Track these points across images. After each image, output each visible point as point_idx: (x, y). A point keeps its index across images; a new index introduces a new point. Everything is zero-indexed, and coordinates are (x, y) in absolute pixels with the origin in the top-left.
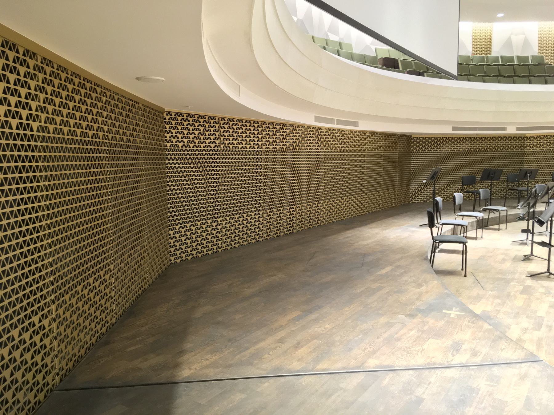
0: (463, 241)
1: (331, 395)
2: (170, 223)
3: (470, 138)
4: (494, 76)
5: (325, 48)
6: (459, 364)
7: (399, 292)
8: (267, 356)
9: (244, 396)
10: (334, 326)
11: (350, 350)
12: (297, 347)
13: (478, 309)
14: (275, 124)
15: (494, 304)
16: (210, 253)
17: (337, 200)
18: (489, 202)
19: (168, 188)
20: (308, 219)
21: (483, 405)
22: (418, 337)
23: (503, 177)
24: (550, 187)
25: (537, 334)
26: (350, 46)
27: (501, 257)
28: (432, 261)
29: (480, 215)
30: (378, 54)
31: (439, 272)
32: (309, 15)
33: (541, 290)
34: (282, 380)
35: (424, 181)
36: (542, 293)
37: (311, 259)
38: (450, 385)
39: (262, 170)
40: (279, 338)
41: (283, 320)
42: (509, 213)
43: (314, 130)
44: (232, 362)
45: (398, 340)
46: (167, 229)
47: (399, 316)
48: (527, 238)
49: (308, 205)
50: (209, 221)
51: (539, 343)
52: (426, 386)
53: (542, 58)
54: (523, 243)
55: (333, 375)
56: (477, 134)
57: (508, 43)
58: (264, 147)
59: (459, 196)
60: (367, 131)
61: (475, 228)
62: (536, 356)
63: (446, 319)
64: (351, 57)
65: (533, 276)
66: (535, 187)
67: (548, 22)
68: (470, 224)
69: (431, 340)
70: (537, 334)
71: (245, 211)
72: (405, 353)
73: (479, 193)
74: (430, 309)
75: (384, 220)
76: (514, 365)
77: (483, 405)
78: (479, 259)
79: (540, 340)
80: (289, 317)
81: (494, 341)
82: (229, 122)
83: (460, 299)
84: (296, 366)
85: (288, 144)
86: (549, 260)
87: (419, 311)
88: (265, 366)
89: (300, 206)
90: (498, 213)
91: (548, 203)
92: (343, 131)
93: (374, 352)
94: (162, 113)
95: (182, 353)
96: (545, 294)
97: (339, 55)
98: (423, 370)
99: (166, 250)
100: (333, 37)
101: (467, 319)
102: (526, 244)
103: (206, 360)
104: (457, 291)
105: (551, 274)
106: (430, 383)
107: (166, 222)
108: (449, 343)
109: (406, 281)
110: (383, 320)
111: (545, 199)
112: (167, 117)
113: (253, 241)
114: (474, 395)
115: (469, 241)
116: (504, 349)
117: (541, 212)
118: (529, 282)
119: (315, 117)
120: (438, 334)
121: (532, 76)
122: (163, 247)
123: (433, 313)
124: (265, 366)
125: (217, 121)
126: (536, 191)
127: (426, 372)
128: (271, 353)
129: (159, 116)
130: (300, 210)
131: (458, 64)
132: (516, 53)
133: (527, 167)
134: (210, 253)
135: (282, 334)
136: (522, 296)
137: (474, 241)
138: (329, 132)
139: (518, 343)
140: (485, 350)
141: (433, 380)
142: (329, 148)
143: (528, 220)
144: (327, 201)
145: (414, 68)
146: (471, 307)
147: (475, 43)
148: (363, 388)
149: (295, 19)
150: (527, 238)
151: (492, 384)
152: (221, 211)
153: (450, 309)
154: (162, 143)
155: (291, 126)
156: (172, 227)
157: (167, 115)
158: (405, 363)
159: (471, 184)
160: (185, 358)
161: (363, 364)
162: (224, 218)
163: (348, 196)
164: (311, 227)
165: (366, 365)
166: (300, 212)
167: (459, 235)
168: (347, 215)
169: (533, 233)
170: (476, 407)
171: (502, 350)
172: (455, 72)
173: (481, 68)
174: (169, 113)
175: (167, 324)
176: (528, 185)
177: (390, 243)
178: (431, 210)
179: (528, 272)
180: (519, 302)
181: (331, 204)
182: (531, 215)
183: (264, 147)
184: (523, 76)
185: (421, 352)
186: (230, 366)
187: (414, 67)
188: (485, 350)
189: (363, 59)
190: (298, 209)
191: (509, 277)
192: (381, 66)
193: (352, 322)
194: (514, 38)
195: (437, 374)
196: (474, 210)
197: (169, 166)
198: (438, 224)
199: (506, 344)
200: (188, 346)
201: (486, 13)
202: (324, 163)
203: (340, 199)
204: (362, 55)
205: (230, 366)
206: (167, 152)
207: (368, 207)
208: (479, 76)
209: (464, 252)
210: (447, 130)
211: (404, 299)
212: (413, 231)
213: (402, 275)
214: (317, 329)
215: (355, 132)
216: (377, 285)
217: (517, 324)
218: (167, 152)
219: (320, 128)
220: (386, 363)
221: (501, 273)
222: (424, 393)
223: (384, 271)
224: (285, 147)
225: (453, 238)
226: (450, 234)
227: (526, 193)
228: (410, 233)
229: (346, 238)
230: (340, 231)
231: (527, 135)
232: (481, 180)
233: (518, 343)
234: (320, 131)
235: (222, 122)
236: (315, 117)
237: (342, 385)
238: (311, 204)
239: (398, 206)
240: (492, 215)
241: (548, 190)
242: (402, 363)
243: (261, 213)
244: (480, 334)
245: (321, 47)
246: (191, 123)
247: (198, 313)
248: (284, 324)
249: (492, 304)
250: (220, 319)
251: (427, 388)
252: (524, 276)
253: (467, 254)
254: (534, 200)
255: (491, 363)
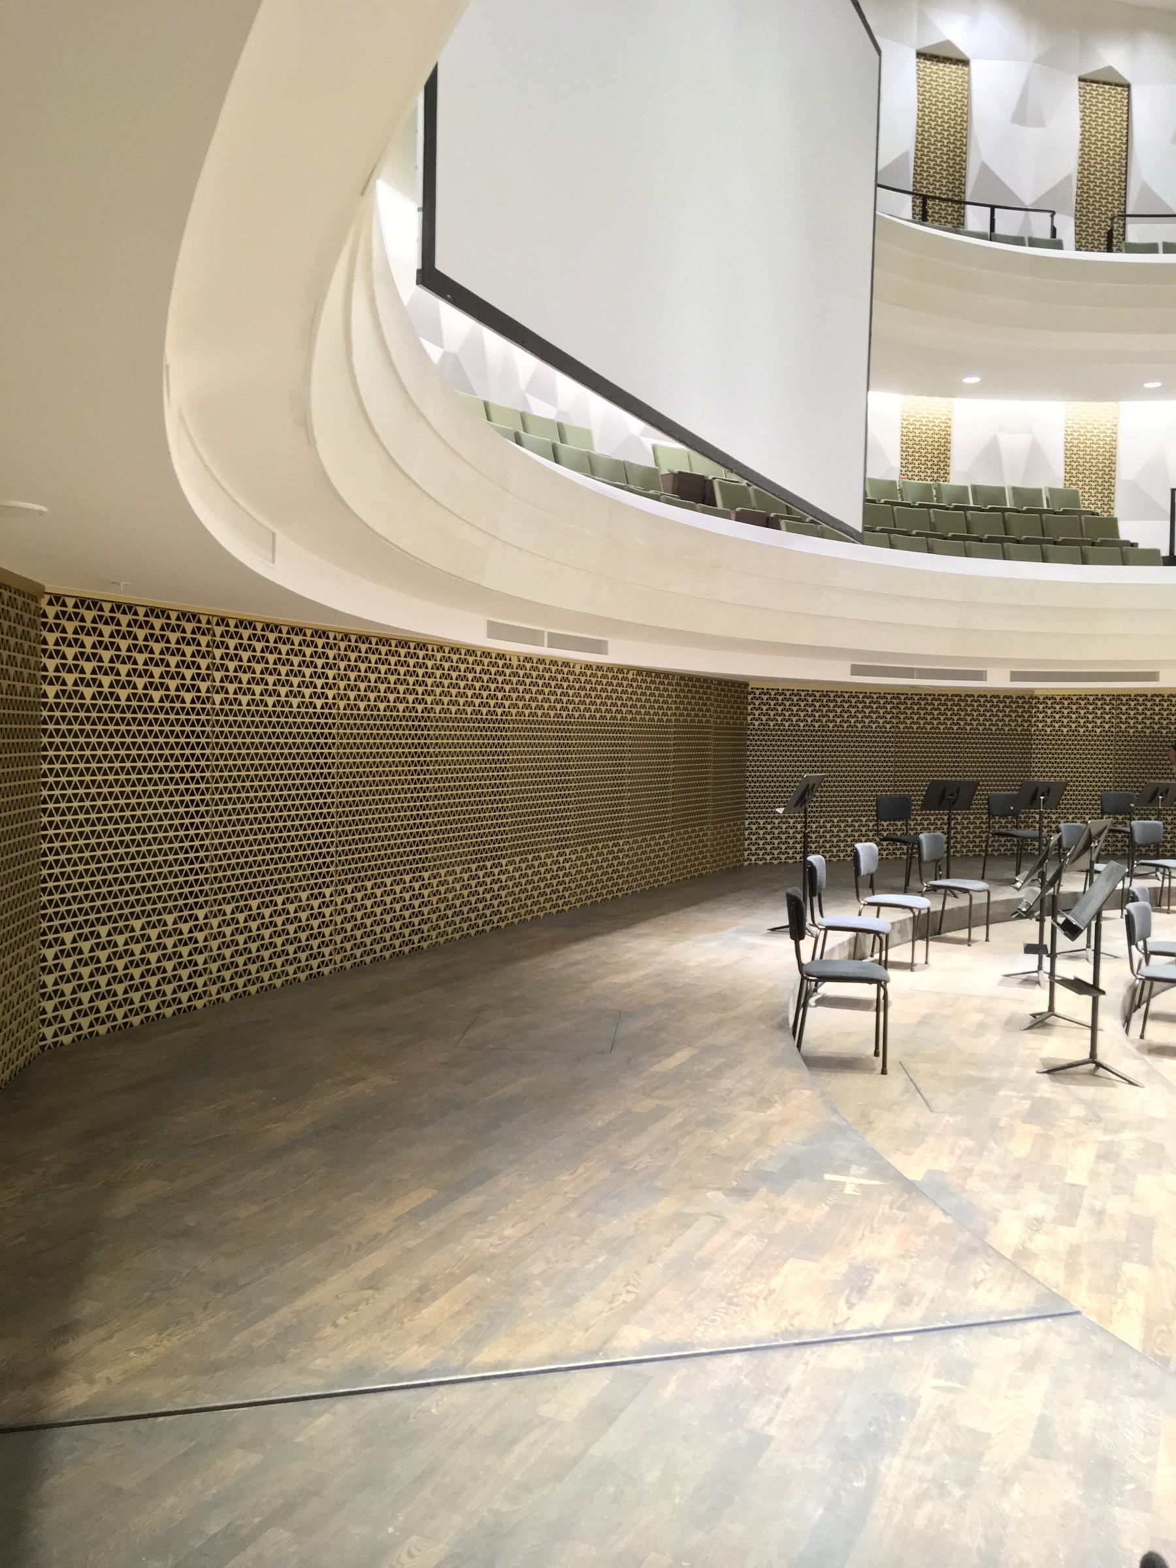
0: (877, 976)
1: (513, 1442)
2: (45, 872)
3: (896, 696)
4: (954, 538)
5: (518, 440)
6: (866, 1330)
7: (711, 1122)
8: (329, 1330)
9: (255, 1458)
10: (527, 1231)
11: (573, 1300)
12: (418, 1300)
13: (915, 1166)
14: (374, 641)
15: (958, 1152)
16: (168, 1012)
17: (547, 857)
18: (944, 867)
19: (45, 793)
20: (465, 909)
21: (927, 1448)
22: (759, 1255)
23: (979, 801)
24: (1094, 832)
25: (1067, 1235)
26: (587, 434)
27: (977, 1017)
28: (797, 1031)
29: (921, 902)
30: (661, 461)
31: (820, 1063)
32: (475, 346)
33: (1077, 1111)
34: (372, 1402)
35: (780, 811)
36: (1078, 1118)
37: (468, 1028)
38: (840, 1392)
39: (334, 731)
40: (366, 1272)
41: (380, 1219)
42: (993, 898)
43: (486, 661)
44: (223, 1354)
45: (705, 1264)
46: (37, 942)
47: (710, 1194)
48: (1040, 968)
49: (464, 871)
50: (170, 919)
51: (1072, 1260)
52: (776, 1399)
53: (1073, 497)
54: (1029, 981)
55: (519, 1381)
56: (913, 687)
57: (991, 453)
58: (342, 704)
59: (867, 850)
60: (630, 669)
61: (910, 937)
62: (1061, 1300)
63: (831, 1199)
64: (589, 465)
65: (1054, 1071)
66: (1058, 831)
67: (1090, 404)
68: (897, 926)
69: (792, 1265)
70: (1067, 1235)
71: (280, 887)
72: (723, 1304)
73: (919, 843)
74: (795, 1171)
75: (674, 914)
76: (1007, 1328)
77: (927, 1448)
78: (920, 1023)
79: (1074, 1251)
80: (399, 1208)
81: (956, 1259)
82: (241, 630)
83: (869, 1138)
84: (414, 1357)
85: (411, 698)
86: (1094, 1028)
87: (763, 1177)
88: (323, 1364)
89: (442, 872)
90: (967, 896)
91: (1090, 872)
92: (566, 664)
93: (638, 1305)
94: (36, 599)
95: (66, 1331)
96: (1086, 1121)
97: (557, 460)
98: (770, 1353)
99: (28, 1006)
100: (540, 409)
101: (888, 1198)
102: (1038, 983)
103: (142, 1350)
104: (863, 1115)
105: (1099, 1065)
106: (787, 1390)
107: (35, 922)
108: (838, 1268)
109: (730, 1091)
110: (665, 1207)
111: (1084, 862)
112: (51, 611)
113: (302, 976)
114: (903, 1419)
115: (892, 973)
116: (982, 1281)
117: (1075, 897)
118: (1047, 1087)
119: (490, 623)
120: (811, 1245)
121: (1049, 542)
122: (22, 970)
123: (798, 1182)
124: (323, 1364)
125: (204, 625)
126: (1060, 840)
127: (778, 1357)
128: (341, 1321)
129: (26, 608)
130: (440, 883)
131: (866, 500)
132: (1011, 478)
133: (1041, 776)
134: (168, 1012)
135: (376, 1260)
136: (1028, 1127)
137: (908, 973)
138: (528, 665)
139: (1018, 1264)
140: (932, 1288)
141: (795, 1378)
142: (527, 712)
143: (1041, 920)
144: (517, 859)
145: (754, 507)
146: (898, 1161)
147: (910, 448)
148: (604, 1414)
149: (435, 353)
150: (1040, 968)
151: (949, 1384)
152: (207, 819)
153: (843, 1169)
154: (32, 687)
155: (422, 646)
156: (50, 937)
157: (50, 603)
158: (722, 1334)
159: (902, 819)
160: (75, 1346)
161: (605, 1342)
162: (216, 908)
163: (579, 844)
164: (472, 932)
165: (615, 1343)
166: (442, 889)
167: (869, 960)
168: (573, 899)
169: (1053, 956)
170: (908, 1456)
171: (976, 1284)
172: (857, 524)
173: (924, 515)
174: (58, 598)
175: (22, 1239)
176: (1040, 822)
177: (687, 981)
178: (797, 891)
179: (1044, 1061)
180: (1021, 1146)
181: (528, 867)
182: (1048, 903)
183: (342, 704)
184: (1027, 541)
185: (765, 1299)
186: (217, 1366)
187: (754, 503)
188: (932, 1288)
189: (622, 475)
190: (435, 882)
191: (995, 1074)
192: (669, 495)
193: (579, 1216)
194: (1007, 442)
195: (807, 1364)
196: (906, 890)
197: (51, 806)
198: (814, 925)
199: (985, 1267)
200: (87, 1307)
201: (936, 372)
202: (513, 753)
203: (555, 853)
204: (618, 462)
205: (217, 1366)
206: (45, 713)
207: (631, 875)
208: (918, 534)
209: (881, 1005)
210: (837, 673)
211: (724, 1142)
212: (751, 947)
213: (718, 1073)
214: (480, 1241)
215: (599, 668)
216: (650, 1104)
217: (1016, 1208)
218: (45, 713)
219: (501, 656)
220: (670, 1337)
221: (974, 1064)
222: (770, 1421)
223: (671, 1063)
224: (401, 707)
225: (852, 968)
226: (845, 954)
227: (1037, 844)
228: (740, 950)
229: (571, 965)
230: (555, 944)
231: (1037, 693)
232: (925, 806)
233: (1018, 1264)
234: (501, 663)
235: (218, 630)
236: (490, 623)
237: (545, 1410)
238: (473, 866)
239: (709, 876)
240: (952, 904)
241: (1090, 839)
242: (712, 1335)
243: (327, 892)
244: (920, 1241)
245: (504, 433)
246: (124, 653)
247: (124, 1205)
248: (384, 1231)
249: (952, 1153)
250: (191, 1220)
251: (778, 1406)
252: (1032, 1072)
253: (890, 1011)
254: (1057, 867)
255: (949, 1324)
